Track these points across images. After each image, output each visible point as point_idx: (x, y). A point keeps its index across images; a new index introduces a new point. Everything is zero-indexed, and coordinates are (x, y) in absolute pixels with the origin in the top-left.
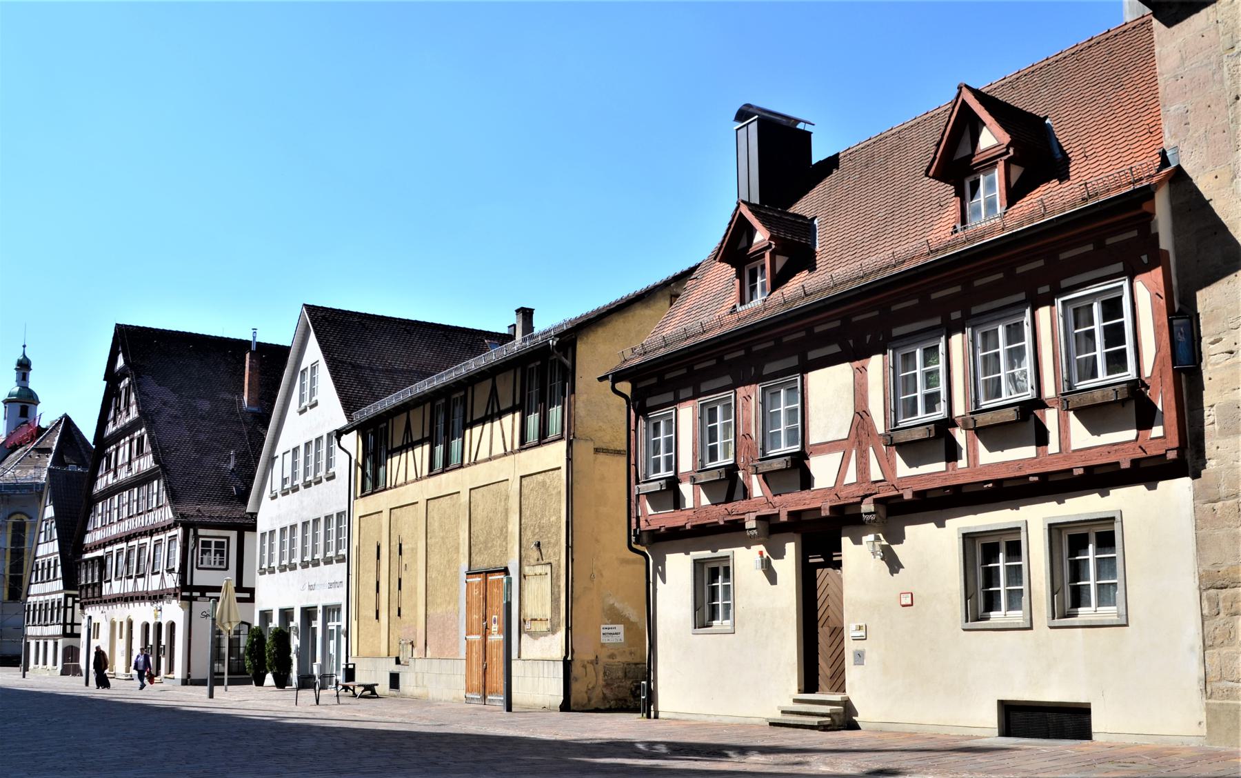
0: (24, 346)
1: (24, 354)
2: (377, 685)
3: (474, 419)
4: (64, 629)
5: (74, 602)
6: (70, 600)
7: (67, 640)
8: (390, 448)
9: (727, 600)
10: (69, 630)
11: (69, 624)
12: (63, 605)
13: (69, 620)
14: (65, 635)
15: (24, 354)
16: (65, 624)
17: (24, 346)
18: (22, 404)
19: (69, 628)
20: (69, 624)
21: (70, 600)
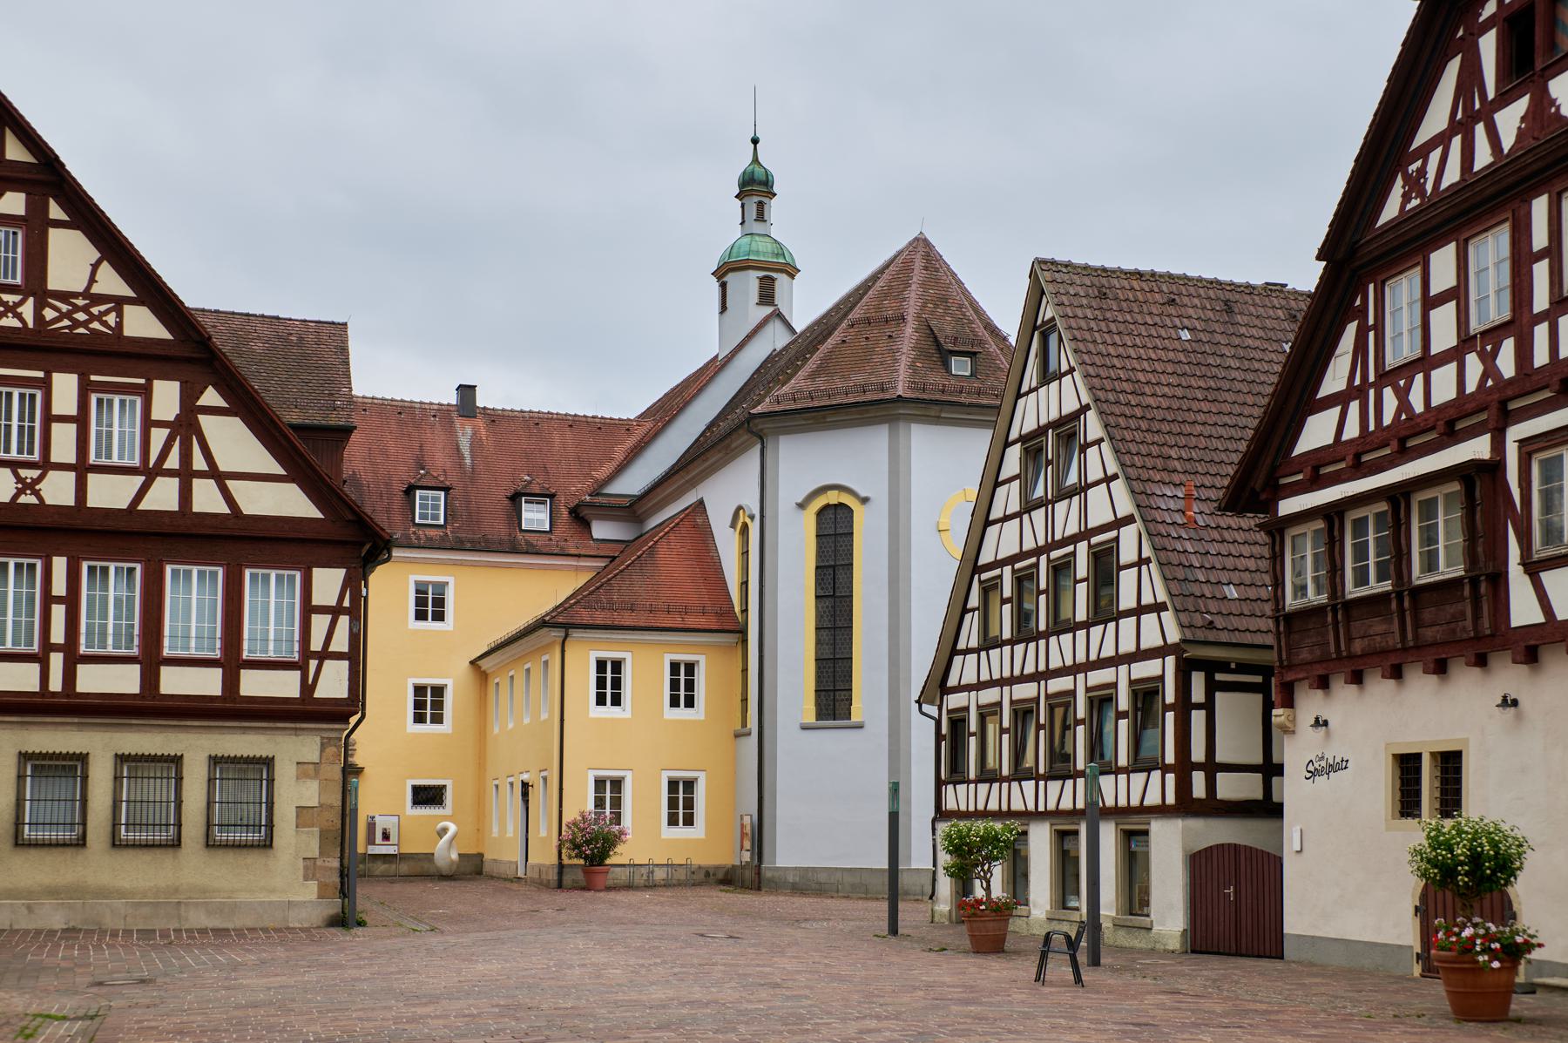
0: (755, 141)
1: (756, 160)
2: (805, 728)
3: (1453, 366)
4: (1184, 786)
5: (1212, 688)
6: (1198, 681)
7: (1197, 824)
8: (1354, 407)
9: (29, 621)
10: (1199, 788)
11: (1198, 767)
12: (1170, 698)
13: (1198, 754)
14: (1185, 806)
15: (756, 160)
16: (1184, 768)
17: (755, 141)
18: (762, 274)
19: (1198, 780)
20: (1198, 767)
21: (1198, 681)
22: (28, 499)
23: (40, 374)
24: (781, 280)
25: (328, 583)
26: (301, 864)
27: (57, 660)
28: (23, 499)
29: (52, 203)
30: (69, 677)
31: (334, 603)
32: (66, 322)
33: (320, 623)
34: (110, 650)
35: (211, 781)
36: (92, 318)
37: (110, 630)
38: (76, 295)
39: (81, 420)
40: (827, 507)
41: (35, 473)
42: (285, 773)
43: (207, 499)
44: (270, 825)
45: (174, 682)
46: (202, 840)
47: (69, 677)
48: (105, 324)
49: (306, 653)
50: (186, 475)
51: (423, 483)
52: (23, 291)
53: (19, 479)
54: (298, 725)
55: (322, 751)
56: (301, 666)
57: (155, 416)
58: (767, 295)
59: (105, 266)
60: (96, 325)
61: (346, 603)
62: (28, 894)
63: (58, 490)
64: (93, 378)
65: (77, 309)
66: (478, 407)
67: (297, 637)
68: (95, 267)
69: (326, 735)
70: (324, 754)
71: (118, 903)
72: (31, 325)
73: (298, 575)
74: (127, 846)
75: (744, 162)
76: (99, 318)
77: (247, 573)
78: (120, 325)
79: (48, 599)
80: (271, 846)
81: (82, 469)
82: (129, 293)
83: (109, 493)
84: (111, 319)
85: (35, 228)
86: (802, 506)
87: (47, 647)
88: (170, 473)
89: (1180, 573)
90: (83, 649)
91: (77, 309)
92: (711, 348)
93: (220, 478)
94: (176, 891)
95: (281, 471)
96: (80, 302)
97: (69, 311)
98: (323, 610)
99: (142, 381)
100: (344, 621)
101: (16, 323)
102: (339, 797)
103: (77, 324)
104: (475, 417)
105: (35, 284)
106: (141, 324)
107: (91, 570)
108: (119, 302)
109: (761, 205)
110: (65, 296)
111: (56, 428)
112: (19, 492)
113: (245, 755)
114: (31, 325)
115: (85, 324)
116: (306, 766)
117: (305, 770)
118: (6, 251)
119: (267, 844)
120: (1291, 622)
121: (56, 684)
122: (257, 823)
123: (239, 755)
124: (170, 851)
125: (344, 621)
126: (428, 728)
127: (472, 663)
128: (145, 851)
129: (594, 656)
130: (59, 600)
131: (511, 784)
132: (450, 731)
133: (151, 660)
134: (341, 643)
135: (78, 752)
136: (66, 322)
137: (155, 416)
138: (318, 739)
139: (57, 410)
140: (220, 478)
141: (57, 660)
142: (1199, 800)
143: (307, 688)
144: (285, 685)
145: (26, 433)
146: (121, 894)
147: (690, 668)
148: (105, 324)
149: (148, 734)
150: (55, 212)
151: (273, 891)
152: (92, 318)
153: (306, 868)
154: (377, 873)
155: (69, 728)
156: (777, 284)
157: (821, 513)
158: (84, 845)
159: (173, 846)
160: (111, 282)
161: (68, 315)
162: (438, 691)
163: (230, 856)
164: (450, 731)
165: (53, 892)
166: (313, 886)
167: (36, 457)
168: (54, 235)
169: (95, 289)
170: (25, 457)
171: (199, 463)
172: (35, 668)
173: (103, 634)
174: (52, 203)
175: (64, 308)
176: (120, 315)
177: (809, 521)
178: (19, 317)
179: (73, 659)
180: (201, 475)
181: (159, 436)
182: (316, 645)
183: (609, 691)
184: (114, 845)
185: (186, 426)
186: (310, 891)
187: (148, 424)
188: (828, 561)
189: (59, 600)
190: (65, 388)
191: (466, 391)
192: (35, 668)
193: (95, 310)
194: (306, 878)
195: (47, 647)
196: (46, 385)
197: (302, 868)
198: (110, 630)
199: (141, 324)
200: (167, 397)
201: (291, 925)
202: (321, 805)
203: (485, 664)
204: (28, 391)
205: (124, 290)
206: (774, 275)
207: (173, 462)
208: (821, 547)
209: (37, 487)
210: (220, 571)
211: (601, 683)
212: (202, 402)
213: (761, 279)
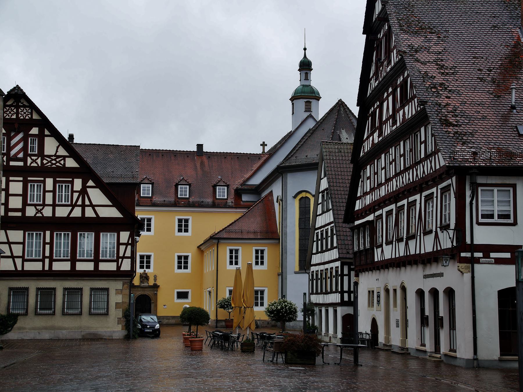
0: (305, 49)
4: (342, 297)
5: (350, 270)
10: (346, 298)
11: (346, 292)
13: (346, 288)
17: (305, 49)
22: (39, 215)
23: (42, 179)
24: (314, 102)
25: (125, 236)
26: (117, 320)
27: (47, 261)
28: (38, 215)
29: (46, 130)
30: (51, 265)
31: (126, 242)
32: (50, 164)
33: (122, 248)
34: (62, 258)
35: (91, 295)
36: (57, 162)
37: (62, 252)
38: (52, 156)
39: (54, 191)
40: (302, 198)
41: (41, 207)
42: (112, 292)
43: (89, 213)
44: (108, 308)
45: (80, 266)
46: (88, 313)
47: (51, 265)
48: (60, 164)
49: (118, 257)
50: (83, 206)
51: (181, 183)
52: (38, 156)
53: (37, 209)
54: (116, 278)
55: (123, 286)
56: (117, 261)
57: (75, 189)
58: (308, 109)
59: (61, 147)
60: (58, 164)
61: (130, 242)
62: (39, 329)
63: (47, 212)
64: (57, 179)
65: (53, 160)
66: (204, 152)
67: (115, 252)
68: (58, 147)
69: (124, 281)
70: (124, 287)
71: (64, 331)
72: (40, 165)
73: (116, 234)
74: (67, 315)
75: (302, 57)
76: (59, 162)
77: (101, 234)
78: (65, 164)
79: (45, 243)
80: (108, 314)
81: (54, 206)
82: (67, 154)
83: (62, 212)
84: (62, 162)
85: (41, 137)
86: (295, 197)
87: (44, 257)
88: (79, 206)
89: (342, 238)
90: (54, 258)
91: (53, 160)
92: (289, 128)
93: (93, 206)
94: (81, 328)
95: (111, 204)
96: (54, 158)
97: (50, 160)
98: (123, 244)
99: (71, 179)
100: (129, 247)
101: (36, 165)
102: (128, 299)
103: (53, 164)
104: (203, 156)
105: (41, 153)
106: (71, 163)
107: (57, 234)
108: (64, 157)
109: (307, 74)
110: (49, 156)
111: (47, 194)
112: (37, 213)
113: (101, 287)
114: (40, 165)
115: (55, 164)
116: (118, 290)
117: (118, 292)
118: (33, 146)
119: (107, 314)
120: (355, 253)
121: (47, 268)
122: (104, 308)
123: (99, 287)
124: (79, 316)
125: (129, 247)
126: (183, 271)
127: (198, 247)
128: (72, 316)
129: (228, 248)
130: (48, 243)
131: (210, 292)
132: (190, 272)
133: (73, 260)
134: (128, 254)
135: (53, 287)
136: (50, 164)
137: (75, 189)
138: (122, 282)
139: (47, 189)
140: (93, 206)
141: (47, 261)
142: (346, 301)
143: (119, 267)
144: (112, 267)
145: (38, 196)
146: (65, 329)
147: (262, 252)
148: (60, 164)
149: (73, 282)
150: (47, 132)
151: (108, 328)
152: (57, 162)
153: (118, 321)
154: (164, 323)
155: (50, 280)
156: (312, 103)
157: (301, 199)
158: (54, 314)
159: (79, 314)
160: (62, 152)
161: (50, 162)
162: (186, 257)
163: (96, 318)
164: (190, 272)
165: (46, 328)
166: (120, 326)
167: (41, 202)
168: (47, 139)
169: (58, 154)
170: (38, 203)
171: (87, 202)
172: (41, 263)
173: (60, 254)
174: (46, 130)
175: (49, 160)
176: (65, 161)
177: (297, 203)
178: (37, 163)
179: (52, 260)
180: (88, 206)
181: (76, 195)
182: (121, 254)
183: (234, 260)
184: (63, 314)
185: (83, 192)
186: (119, 328)
187: (73, 192)
188: (303, 216)
189: (48, 243)
190: (49, 182)
191: (200, 147)
192: (41, 263)
193: (58, 160)
194: (118, 324)
195: (44, 257)
196: (44, 182)
197: (117, 321)
198: (62, 252)
199: (71, 163)
200: (78, 184)
201: (114, 338)
202: (123, 302)
203: (202, 248)
204: (39, 184)
205: (65, 153)
206: (311, 100)
207: (80, 202)
208: (301, 211)
209: (42, 211)
210: (93, 234)
211: (231, 257)
212: (88, 184)
213: (306, 102)
